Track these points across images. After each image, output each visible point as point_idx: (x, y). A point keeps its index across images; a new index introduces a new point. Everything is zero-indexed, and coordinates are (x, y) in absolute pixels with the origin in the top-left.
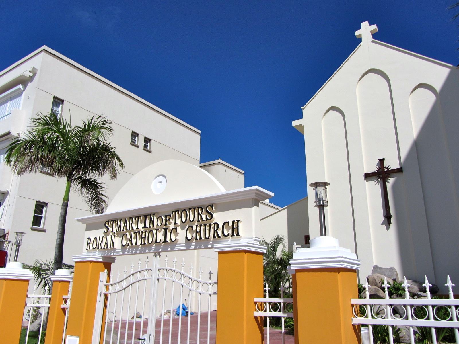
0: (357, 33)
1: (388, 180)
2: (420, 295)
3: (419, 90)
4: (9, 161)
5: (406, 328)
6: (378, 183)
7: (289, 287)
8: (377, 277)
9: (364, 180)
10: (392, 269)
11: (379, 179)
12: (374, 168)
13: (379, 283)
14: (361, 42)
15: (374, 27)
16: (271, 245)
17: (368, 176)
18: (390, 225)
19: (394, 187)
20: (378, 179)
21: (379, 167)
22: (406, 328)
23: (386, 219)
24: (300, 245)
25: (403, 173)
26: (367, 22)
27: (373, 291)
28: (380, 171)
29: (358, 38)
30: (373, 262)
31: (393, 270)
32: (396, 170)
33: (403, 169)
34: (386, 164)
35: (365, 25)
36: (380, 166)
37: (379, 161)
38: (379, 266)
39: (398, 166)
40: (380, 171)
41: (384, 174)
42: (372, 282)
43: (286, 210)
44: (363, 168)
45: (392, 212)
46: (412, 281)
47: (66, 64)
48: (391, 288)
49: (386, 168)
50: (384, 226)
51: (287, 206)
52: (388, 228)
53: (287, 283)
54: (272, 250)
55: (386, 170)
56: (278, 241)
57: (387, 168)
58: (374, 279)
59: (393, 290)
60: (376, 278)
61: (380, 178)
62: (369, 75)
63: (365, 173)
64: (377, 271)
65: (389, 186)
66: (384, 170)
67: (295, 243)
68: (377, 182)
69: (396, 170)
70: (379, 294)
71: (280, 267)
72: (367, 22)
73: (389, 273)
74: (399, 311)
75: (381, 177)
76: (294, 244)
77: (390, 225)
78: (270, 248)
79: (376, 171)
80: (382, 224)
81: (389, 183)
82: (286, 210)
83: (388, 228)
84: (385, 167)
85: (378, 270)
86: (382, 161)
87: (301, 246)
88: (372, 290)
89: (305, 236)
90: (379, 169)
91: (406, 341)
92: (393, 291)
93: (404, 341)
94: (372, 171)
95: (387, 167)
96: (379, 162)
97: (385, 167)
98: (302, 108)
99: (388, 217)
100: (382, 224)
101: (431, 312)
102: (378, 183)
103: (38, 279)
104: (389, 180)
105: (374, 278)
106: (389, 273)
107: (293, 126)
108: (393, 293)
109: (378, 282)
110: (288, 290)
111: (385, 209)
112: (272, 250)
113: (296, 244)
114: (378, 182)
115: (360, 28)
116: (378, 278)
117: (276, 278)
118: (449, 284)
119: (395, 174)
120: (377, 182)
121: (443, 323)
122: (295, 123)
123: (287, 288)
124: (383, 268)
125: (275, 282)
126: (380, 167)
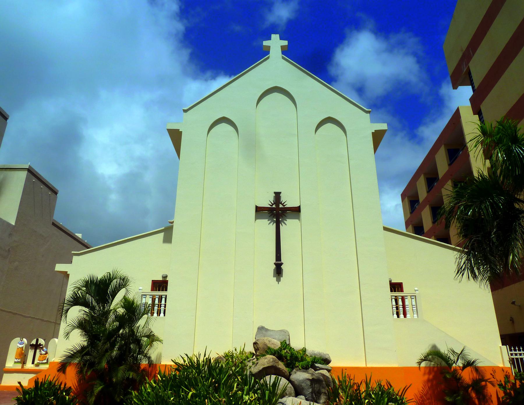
0: (266, 43)
2: (318, 367)
4: (475, 277)
8: (269, 341)
10: (284, 331)
12: (266, 201)
15: (285, 43)
27: (271, 362)
29: (264, 49)
34: (283, 199)
47: (425, 184)
55: (281, 206)
57: (283, 204)
60: (267, 342)
70: (278, 365)
101: (518, 354)
104: (286, 221)
105: (265, 343)
115: (269, 38)
118: (521, 348)
121: (521, 357)
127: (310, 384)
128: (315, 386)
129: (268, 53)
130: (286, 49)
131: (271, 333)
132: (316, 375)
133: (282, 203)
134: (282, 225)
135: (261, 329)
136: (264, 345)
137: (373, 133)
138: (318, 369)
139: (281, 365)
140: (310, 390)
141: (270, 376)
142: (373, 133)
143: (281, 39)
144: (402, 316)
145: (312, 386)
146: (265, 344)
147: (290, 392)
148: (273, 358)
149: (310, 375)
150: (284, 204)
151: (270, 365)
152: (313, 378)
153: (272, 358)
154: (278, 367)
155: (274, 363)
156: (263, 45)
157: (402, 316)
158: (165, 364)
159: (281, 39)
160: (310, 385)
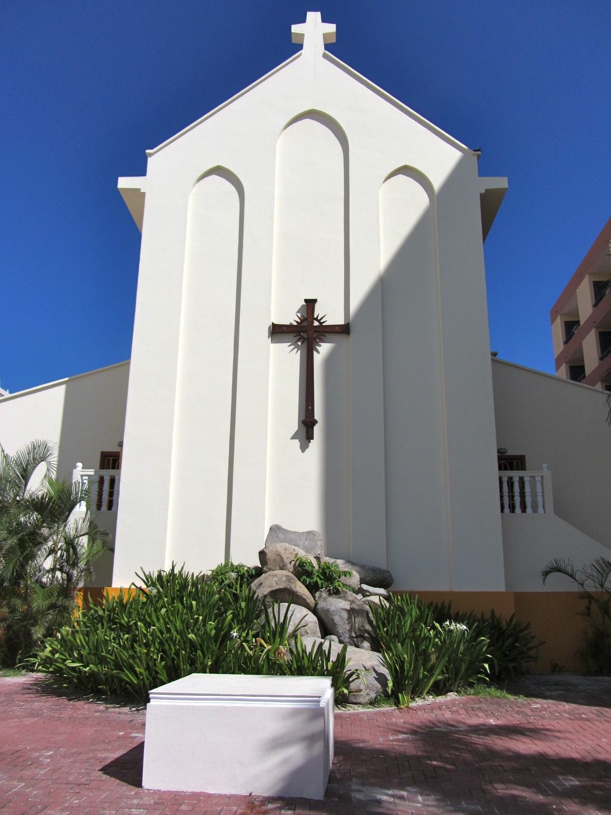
0: (296, 29)
1: (317, 347)
3: (401, 178)
5: (365, 667)
6: (296, 349)
7: (53, 570)
8: (285, 549)
9: (269, 338)
11: (299, 340)
12: (291, 318)
13: (290, 563)
14: (302, 49)
15: (331, 28)
16: (19, 464)
17: (278, 332)
18: (311, 441)
19: (329, 361)
20: (296, 342)
21: (302, 315)
22: (365, 667)
23: (304, 429)
24: (93, 470)
25: (351, 335)
26: (319, 14)
28: (304, 324)
29: (294, 41)
30: (264, 519)
31: (315, 536)
32: (337, 328)
33: (353, 329)
34: (318, 311)
35: (314, 17)
36: (306, 316)
37: (305, 304)
38: (284, 527)
39: (340, 321)
40: (305, 324)
41: (312, 332)
42: (274, 560)
43: (63, 387)
44: (270, 312)
45: (318, 414)
46: (344, 562)
48: (318, 576)
49: (316, 319)
50: (297, 443)
51: (66, 379)
52: (304, 448)
53: (51, 558)
54: (17, 475)
55: (316, 323)
56: (37, 455)
57: (319, 321)
58: (278, 555)
59: (321, 579)
61: (302, 340)
62: (307, 122)
63: (273, 324)
64: (278, 536)
65: (318, 359)
66: (313, 323)
67: (80, 465)
68: (293, 346)
69: (337, 328)
70: (295, 588)
71: (35, 516)
72: (319, 14)
73: (307, 543)
74: (336, 628)
75: (304, 338)
76: (75, 467)
77: (311, 441)
78: (15, 471)
79: (295, 324)
80: (293, 438)
81: (318, 352)
82: (63, 387)
83: (304, 448)
84: (315, 317)
85: (281, 536)
86: (310, 304)
87: (95, 472)
88: (280, 580)
89: (102, 453)
90: (303, 320)
91: (361, 699)
92: (320, 582)
93: (358, 698)
94: (286, 322)
95: (319, 318)
96: (303, 305)
97: (315, 317)
98: (148, 151)
99: (307, 424)
100: (293, 438)
102: (296, 349)
103: (475, 615)
104: (320, 346)
105: (277, 551)
106: (307, 543)
107: (119, 187)
108: (320, 586)
109: (287, 561)
110: (50, 576)
111: (304, 407)
112: (18, 476)
113: (83, 468)
114: (297, 346)
116: (287, 552)
117: (22, 544)
119: (332, 336)
120: (293, 346)
122: (124, 183)
123: (48, 571)
124: (292, 530)
125: (18, 557)
126: (306, 317)
127: (348, 617)
128: (356, 619)
129: (300, 47)
130: (333, 40)
131: (292, 537)
132: (358, 603)
133: (319, 318)
134: (289, 346)
135: (275, 530)
136: (276, 556)
137: (481, 194)
138: (368, 594)
139: (301, 589)
140: (348, 627)
141: (286, 604)
142: (481, 194)
143: (324, 20)
144: (518, 509)
145: (350, 620)
146: (278, 553)
147: (313, 630)
148: (287, 576)
149: (348, 603)
150: (322, 321)
151: (282, 587)
152: (352, 607)
153: (285, 576)
154: (295, 590)
155: (287, 583)
156: (292, 31)
157: (518, 509)
158: (120, 587)
159: (324, 20)
160: (347, 618)
